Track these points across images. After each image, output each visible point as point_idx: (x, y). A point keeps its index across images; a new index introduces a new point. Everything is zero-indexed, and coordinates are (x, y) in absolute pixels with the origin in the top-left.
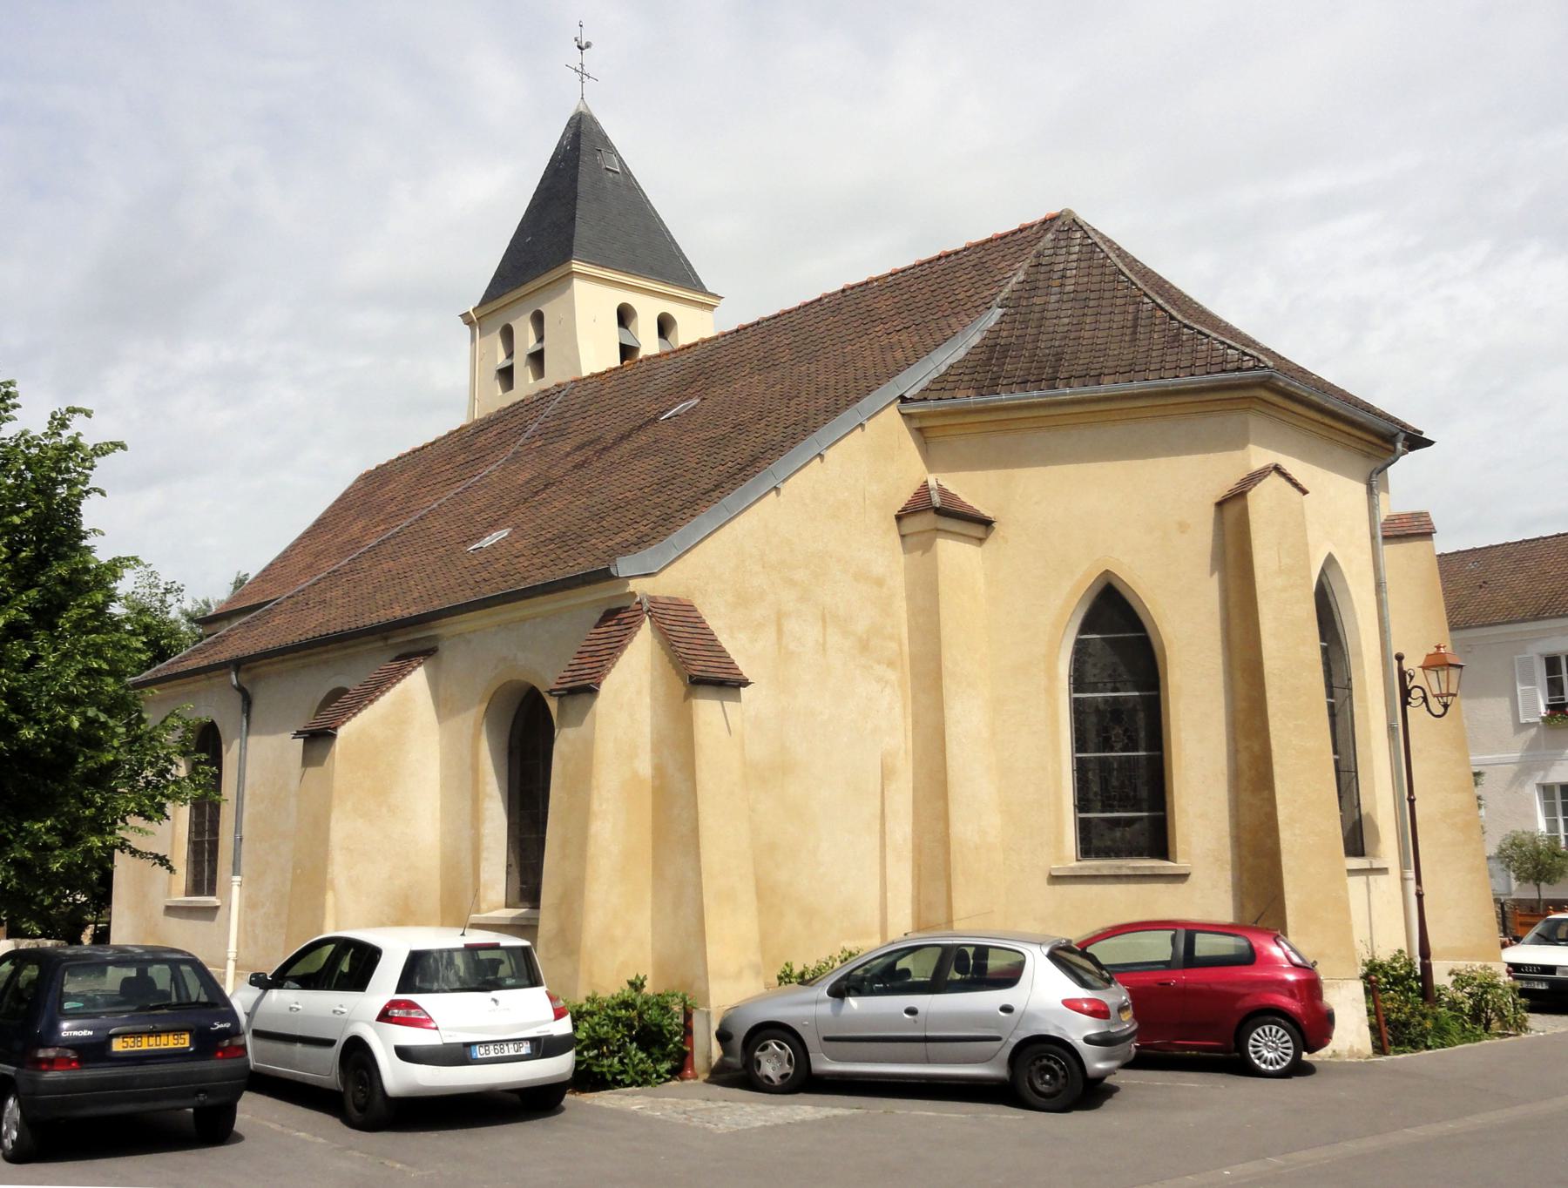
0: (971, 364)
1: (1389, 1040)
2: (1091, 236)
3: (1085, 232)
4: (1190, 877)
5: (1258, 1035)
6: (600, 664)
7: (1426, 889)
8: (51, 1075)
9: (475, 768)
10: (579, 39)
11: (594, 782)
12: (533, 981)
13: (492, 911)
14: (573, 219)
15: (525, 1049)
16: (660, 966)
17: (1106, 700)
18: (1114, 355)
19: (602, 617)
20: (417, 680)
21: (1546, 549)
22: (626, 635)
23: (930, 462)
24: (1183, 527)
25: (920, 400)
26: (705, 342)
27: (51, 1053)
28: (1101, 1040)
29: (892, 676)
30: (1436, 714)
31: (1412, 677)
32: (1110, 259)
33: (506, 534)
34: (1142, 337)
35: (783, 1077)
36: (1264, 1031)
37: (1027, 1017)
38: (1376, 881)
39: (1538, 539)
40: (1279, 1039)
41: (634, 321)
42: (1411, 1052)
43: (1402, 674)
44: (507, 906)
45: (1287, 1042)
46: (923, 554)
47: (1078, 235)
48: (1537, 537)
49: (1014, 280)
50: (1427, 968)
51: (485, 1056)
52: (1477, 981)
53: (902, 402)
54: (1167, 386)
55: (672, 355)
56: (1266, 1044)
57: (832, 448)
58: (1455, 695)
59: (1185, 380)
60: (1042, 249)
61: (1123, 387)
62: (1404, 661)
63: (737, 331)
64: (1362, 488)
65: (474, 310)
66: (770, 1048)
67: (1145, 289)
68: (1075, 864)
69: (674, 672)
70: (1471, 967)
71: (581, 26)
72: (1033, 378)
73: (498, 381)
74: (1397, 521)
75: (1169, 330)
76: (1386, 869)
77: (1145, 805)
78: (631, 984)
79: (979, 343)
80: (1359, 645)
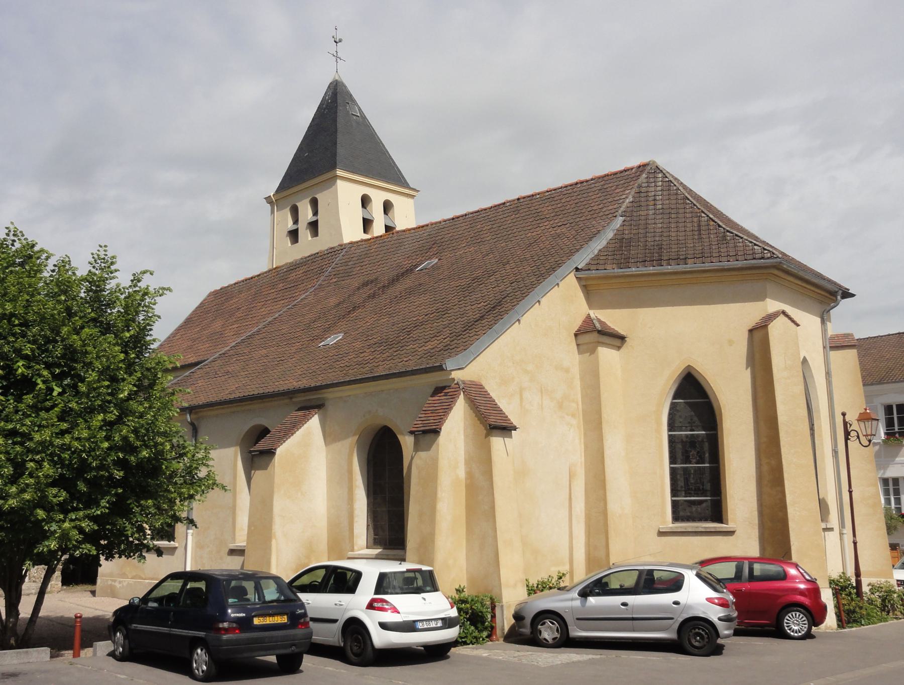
0: (610, 250)
1: (845, 620)
2: (667, 176)
3: (664, 174)
4: (736, 533)
5: (789, 617)
6: (439, 417)
7: (858, 539)
8: (225, 637)
9: (350, 472)
10: (335, 37)
11: (439, 482)
12: (435, 589)
13: (359, 550)
14: (336, 144)
15: (440, 624)
16: (472, 579)
17: (687, 436)
18: (691, 247)
19: (434, 391)
20: (314, 423)
21: (883, 343)
22: (452, 401)
23: (591, 305)
24: (731, 343)
25: (587, 270)
26: (433, 224)
27: (226, 625)
28: (726, 619)
29: (574, 422)
30: (864, 445)
31: (851, 425)
32: (680, 190)
33: (341, 337)
34: (704, 236)
35: (554, 639)
36: (792, 615)
37: (687, 607)
38: (828, 535)
39: (877, 337)
40: (800, 619)
41: (370, 204)
42: (856, 627)
43: (845, 423)
44: (367, 547)
45: (804, 621)
46: (590, 355)
47: (660, 175)
48: (877, 335)
49: (627, 201)
50: (859, 582)
51: (422, 627)
52: (884, 589)
53: (576, 271)
54: (723, 266)
55: (413, 231)
56: (793, 622)
57: (544, 297)
58: (875, 435)
59: (734, 264)
60: (641, 183)
61: (699, 266)
62: (846, 416)
63: (453, 219)
64: (818, 320)
65: (273, 195)
66: (546, 624)
67: (702, 209)
68: (671, 525)
69: (479, 422)
70: (880, 582)
71: (336, 29)
72: (648, 259)
73: (288, 238)
74: (836, 338)
75: (719, 233)
76: (833, 528)
77: (709, 494)
78: (457, 590)
79: (613, 237)
80: (818, 406)
